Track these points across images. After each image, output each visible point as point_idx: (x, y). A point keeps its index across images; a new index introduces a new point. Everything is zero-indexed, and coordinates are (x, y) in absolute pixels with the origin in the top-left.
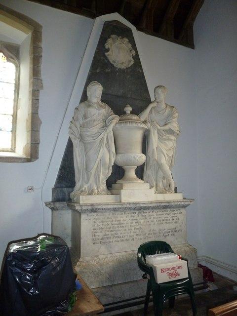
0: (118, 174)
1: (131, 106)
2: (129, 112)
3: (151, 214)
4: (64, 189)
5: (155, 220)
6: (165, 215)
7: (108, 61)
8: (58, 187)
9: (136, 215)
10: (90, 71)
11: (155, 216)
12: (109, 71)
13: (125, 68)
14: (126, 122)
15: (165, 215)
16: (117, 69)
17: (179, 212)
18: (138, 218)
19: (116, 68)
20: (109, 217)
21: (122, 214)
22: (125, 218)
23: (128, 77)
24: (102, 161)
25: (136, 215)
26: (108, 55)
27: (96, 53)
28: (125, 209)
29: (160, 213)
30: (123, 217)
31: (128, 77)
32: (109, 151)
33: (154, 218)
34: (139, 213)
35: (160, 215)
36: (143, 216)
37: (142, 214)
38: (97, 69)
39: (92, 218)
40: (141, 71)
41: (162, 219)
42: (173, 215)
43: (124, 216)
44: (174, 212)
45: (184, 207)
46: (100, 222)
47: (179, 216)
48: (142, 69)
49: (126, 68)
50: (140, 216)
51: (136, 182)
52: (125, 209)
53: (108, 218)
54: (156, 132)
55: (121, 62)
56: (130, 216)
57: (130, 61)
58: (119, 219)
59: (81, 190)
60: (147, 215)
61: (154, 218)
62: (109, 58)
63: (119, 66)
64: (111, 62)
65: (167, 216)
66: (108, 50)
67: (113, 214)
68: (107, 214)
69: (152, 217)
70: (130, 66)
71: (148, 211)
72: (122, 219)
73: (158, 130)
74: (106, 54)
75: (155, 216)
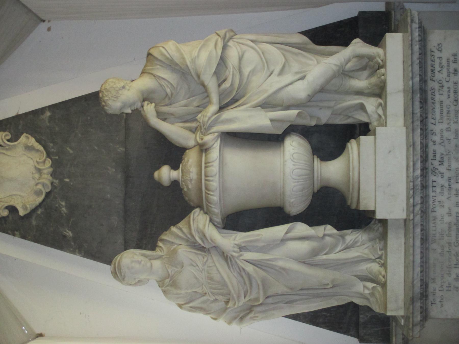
0: (334, 209)
1: (158, 168)
2: (175, 174)
3: (437, 138)
4: (361, 320)
5: (453, 127)
6: (444, 98)
7: (40, 205)
8: (358, 332)
9: (440, 181)
10: (73, 252)
11: (444, 126)
12: (63, 203)
13: (49, 162)
14: (207, 188)
15: (444, 98)
16: (56, 181)
17: (437, 54)
18: (447, 175)
19: (52, 183)
20: (439, 251)
21: (435, 218)
22: (445, 210)
23: (71, 152)
24: (307, 260)
25: (440, 181)
26: (25, 208)
27: (24, 237)
28: (424, 213)
29: (437, 111)
30: (442, 217)
31: (71, 152)
32: (284, 241)
33: (448, 130)
34: (434, 171)
35: (441, 113)
36: (441, 163)
37: (436, 163)
38: (65, 236)
39: (439, 294)
40: (48, 114)
41: (453, 108)
42: (445, 71)
43: (440, 212)
44: (437, 68)
45: (423, 32)
46: (449, 274)
47: (446, 54)
48: (42, 110)
49: (48, 155)
50: (442, 169)
51: (355, 194)
52: (424, 213)
53: (442, 254)
54: (227, 114)
55: (37, 176)
56: (439, 198)
57: (29, 148)
58: (445, 227)
59: (369, 297)
60: (440, 150)
61: (448, 130)
62: (30, 207)
63: (47, 179)
64: (40, 199)
65: (445, 89)
66: (12, 209)
67: (434, 241)
68: (433, 257)
69: (446, 134)
70: (41, 148)
71: (431, 147)
72: (447, 219)
73: (222, 108)
74: (22, 213)
75: (444, 126)
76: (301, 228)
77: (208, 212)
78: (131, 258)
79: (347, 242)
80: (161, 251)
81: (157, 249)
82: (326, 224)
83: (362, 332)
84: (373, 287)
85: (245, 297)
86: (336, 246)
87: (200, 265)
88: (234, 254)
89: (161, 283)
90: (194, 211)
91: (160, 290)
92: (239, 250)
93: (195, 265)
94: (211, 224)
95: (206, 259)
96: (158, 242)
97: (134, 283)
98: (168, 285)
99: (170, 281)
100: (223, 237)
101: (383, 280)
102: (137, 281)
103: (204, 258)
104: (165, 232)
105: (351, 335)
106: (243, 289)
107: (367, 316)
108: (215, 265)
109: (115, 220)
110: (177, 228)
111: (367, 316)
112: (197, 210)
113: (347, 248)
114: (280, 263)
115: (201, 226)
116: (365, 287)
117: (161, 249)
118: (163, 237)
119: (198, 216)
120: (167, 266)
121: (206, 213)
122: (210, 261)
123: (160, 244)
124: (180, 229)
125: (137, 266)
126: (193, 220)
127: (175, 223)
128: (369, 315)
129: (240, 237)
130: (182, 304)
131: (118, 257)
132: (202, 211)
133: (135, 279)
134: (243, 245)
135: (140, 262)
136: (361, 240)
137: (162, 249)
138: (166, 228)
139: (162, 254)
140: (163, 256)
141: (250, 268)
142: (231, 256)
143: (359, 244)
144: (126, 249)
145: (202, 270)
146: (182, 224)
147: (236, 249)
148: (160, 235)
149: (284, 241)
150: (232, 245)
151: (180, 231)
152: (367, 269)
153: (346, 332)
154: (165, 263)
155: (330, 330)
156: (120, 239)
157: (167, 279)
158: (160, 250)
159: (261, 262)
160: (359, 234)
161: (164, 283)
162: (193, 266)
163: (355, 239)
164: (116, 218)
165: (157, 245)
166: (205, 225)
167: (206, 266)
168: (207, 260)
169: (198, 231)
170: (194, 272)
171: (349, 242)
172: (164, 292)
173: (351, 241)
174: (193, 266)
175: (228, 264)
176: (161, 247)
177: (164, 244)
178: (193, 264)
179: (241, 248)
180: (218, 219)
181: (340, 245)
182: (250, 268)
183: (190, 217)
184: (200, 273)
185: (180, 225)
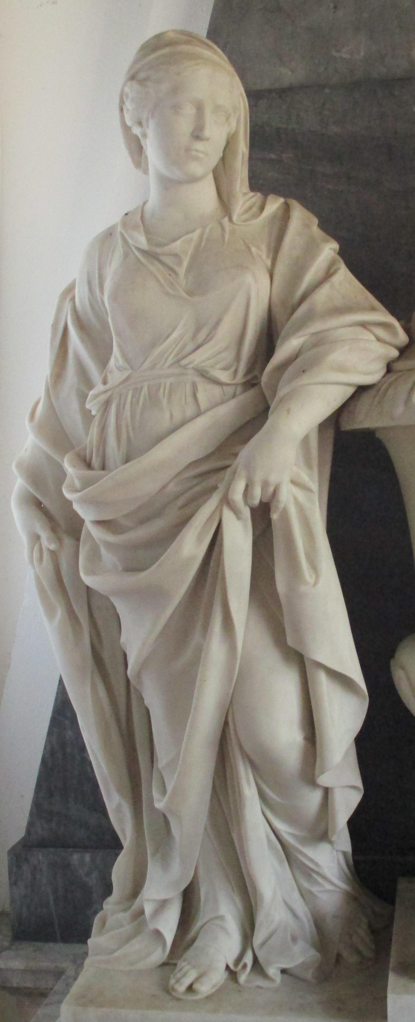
4: (75, 857)
8: (42, 844)
32: (299, 660)
76: (344, 716)
77: (392, 377)
78: (219, 97)
79: (309, 851)
80: (247, 211)
81: (257, 197)
82: (366, 790)
83: (40, 857)
84: (158, 934)
85: (99, 523)
86: (290, 817)
87: (199, 358)
88: (239, 487)
89: (137, 219)
90: (396, 324)
91: (115, 218)
92: (256, 502)
93: (201, 336)
94: (350, 391)
95: (224, 377)
96: (282, 200)
97: (129, 123)
98: (142, 247)
99: (143, 252)
100: (306, 440)
101: (182, 988)
102: (137, 131)
103: (225, 369)
104: (316, 221)
105: (31, 824)
106: (126, 516)
107: (88, 874)
108: (199, 413)
109: (354, 51)
110: (332, 263)
111: (88, 874)
112: (402, 338)
113: (288, 854)
114: (216, 649)
115: (338, 356)
116: (163, 905)
117: (255, 209)
118: (299, 215)
119: (379, 339)
120: (195, 235)
121: (389, 369)
122: (217, 391)
123: (274, 205)
124: (328, 274)
125: (184, 125)
126: (364, 325)
127: (352, 257)
128: (93, 880)
129: (304, 503)
130: (73, 299)
131: (219, 56)
132: (395, 353)
133: (140, 124)
134: (275, 516)
135: (197, 135)
136: (315, 889)
137: (255, 216)
138: (329, 226)
139: (235, 218)
140: (230, 220)
141: (191, 546)
142: (233, 467)
143: (305, 884)
144: (254, 96)
145: (185, 367)
146: (345, 281)
147: (257, 495)
148: (309, 205)
149: (299, 660)
150: (273, 479)
151: (321, 274)
152: (222, 918)
153: (39, 809)
154: (204, 227)
155: (44, 762)
156: (290, 74)
157: (149, 240)
158: (250, 208)
159: (214, 584)
160: (336, 881)
161: (135, 227)
162: (198, 330)
163: (318, 873)
164: (362, 54)
165: (271, 197)
166: (341, 369)
167: (197, 379)
168: (217, 382)
169: (320, 342)
170: (175, 335)
171: (305, 856)
172: (109, 234)
173: (312, 861)
174: (198, 330)
175: (207, 457)
176: (262, 209)
177: (274, 217)
178: (203, 331)
179: (263, 517)
180: (364, 419)
181: (291, 830)
182: (191, 546)
183: (373, 309)
184: (170, 360)
185: (343, 274)
